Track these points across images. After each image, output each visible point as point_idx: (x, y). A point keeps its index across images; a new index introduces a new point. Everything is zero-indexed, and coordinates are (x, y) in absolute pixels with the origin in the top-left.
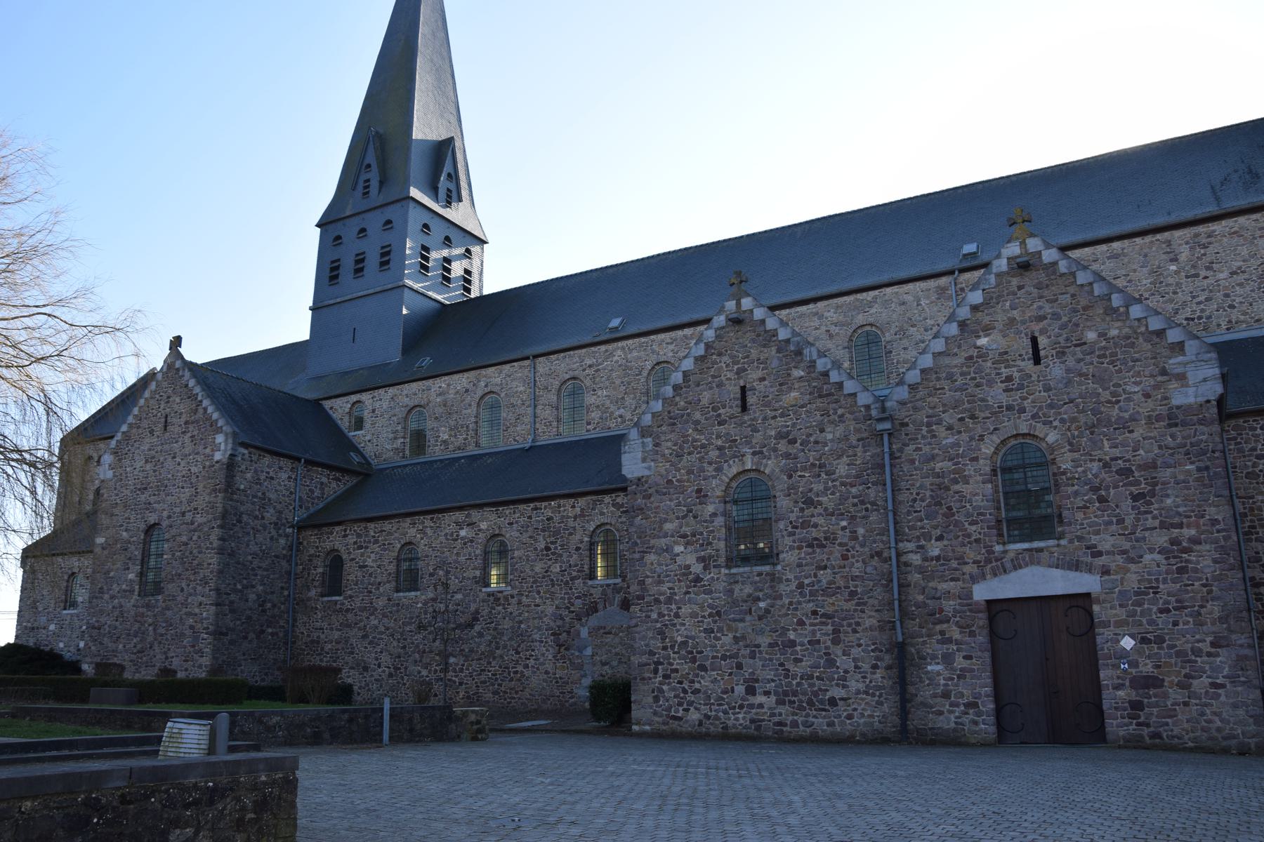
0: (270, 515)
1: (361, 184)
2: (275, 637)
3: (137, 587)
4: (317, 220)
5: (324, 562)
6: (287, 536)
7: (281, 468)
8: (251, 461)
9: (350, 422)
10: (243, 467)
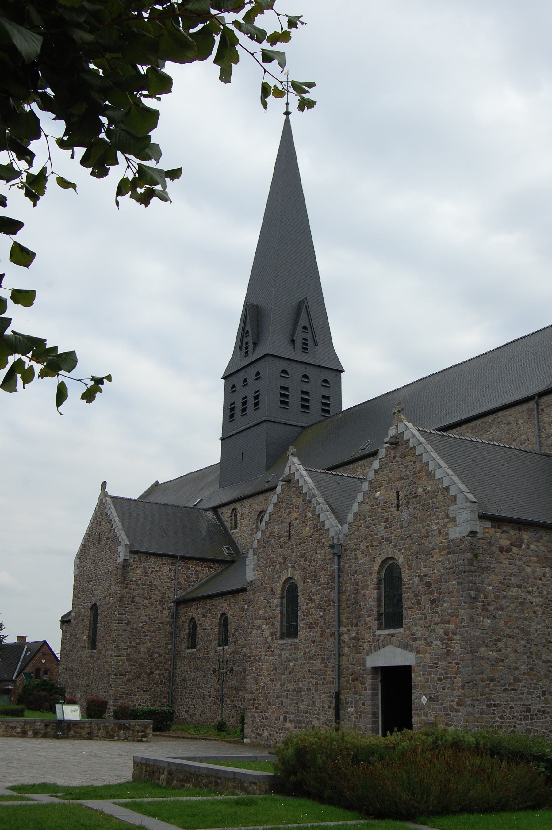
0: (156, 596)
1: (244, 346)
2: (161, 677)
3: (87, 644)
4: (222, 372)
5: (189, 625)
6: (169, 609)
7: (163, 564)
8: (141, 562)
9: (231, 523)
10: (135, 566)
